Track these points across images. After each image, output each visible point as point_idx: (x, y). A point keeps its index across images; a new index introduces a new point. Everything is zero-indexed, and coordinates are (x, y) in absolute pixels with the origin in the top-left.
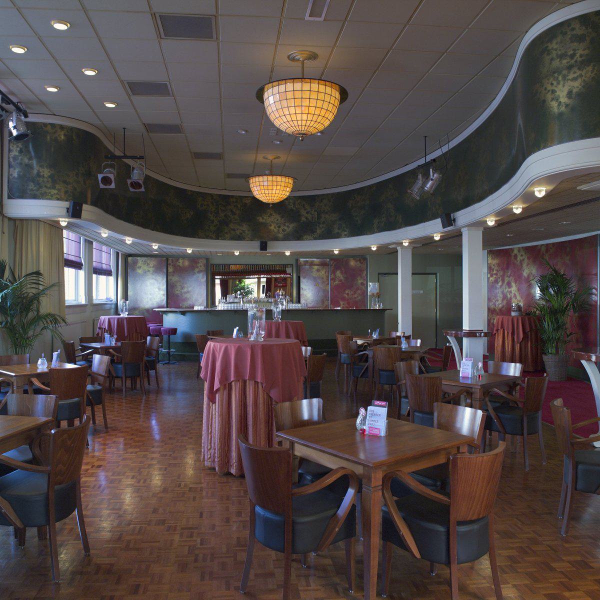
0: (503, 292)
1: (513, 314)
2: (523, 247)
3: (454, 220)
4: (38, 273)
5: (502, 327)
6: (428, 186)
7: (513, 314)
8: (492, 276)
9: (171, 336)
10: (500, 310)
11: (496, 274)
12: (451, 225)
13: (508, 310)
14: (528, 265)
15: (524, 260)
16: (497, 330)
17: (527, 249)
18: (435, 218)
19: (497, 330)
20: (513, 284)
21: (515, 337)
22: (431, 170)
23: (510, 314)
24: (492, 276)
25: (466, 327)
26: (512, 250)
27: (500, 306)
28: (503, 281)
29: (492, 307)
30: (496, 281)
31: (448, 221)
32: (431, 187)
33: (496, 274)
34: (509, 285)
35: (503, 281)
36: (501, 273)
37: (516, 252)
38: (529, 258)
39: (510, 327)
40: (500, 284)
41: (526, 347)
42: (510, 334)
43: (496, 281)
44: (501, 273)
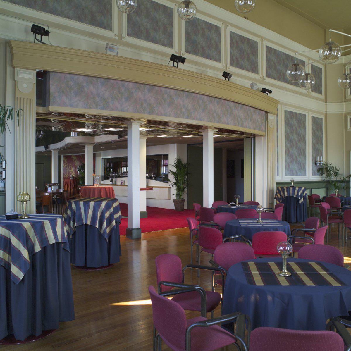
0: (68, 171)
1: (71, 179)
2: (75, 155)
3: (49, 147)
4: (120, 223)
5: (67, 183)
6: (40, 136)
7: (71, 179)
8: (65, 165)
9: (309, 190)
10: (68, 178)
11: (66, 164)
12: (48, 149)
13: (69, 178)
14: (77, 161)
15: (75, 160)
16: (65, 184)
17: (77, 156)
18: (43, 146)
19: (65, 184)
20: (72, 168)
21: (71, 187)
22: (41, 131)
23: (70, 179)
24: (65, 165)
25: (53, 182)
26: (72, 156)
27: (68, 176)
28: (69, 167)
29: (65, 177)
30: (66, 167)
31: (47, 147)
32: (41, 136)
33: (66, 164)
34: (71, 169)
35: (69, 167)
36: (68, 164)
37: (73, 157)
38: (77, 159)
39: (70, 183)
40: (67, 168)
41: (75, 190)
42: (69, 186)
43: (66, 167)
44: (68, 164)
